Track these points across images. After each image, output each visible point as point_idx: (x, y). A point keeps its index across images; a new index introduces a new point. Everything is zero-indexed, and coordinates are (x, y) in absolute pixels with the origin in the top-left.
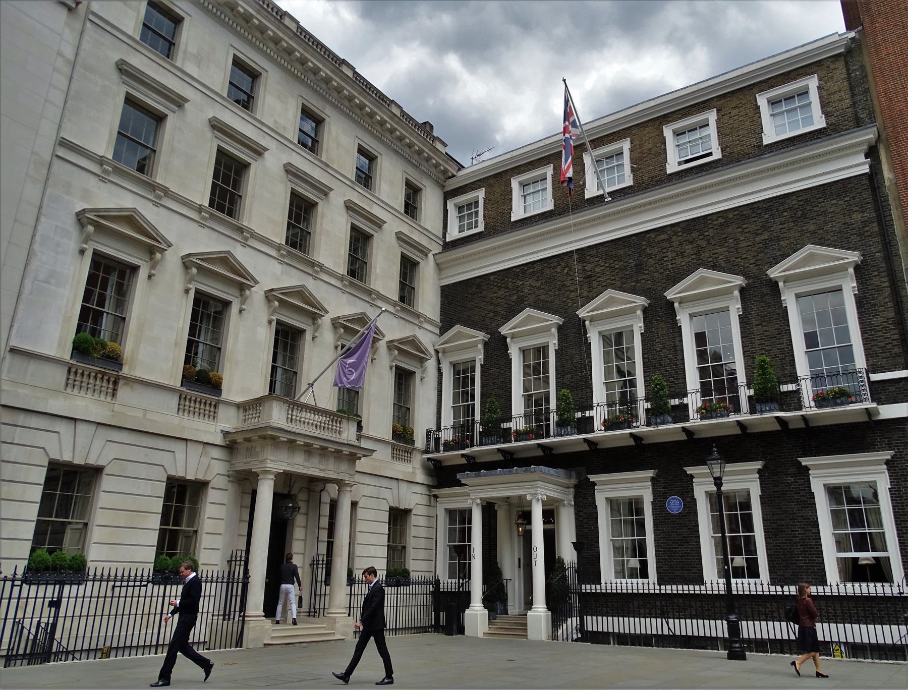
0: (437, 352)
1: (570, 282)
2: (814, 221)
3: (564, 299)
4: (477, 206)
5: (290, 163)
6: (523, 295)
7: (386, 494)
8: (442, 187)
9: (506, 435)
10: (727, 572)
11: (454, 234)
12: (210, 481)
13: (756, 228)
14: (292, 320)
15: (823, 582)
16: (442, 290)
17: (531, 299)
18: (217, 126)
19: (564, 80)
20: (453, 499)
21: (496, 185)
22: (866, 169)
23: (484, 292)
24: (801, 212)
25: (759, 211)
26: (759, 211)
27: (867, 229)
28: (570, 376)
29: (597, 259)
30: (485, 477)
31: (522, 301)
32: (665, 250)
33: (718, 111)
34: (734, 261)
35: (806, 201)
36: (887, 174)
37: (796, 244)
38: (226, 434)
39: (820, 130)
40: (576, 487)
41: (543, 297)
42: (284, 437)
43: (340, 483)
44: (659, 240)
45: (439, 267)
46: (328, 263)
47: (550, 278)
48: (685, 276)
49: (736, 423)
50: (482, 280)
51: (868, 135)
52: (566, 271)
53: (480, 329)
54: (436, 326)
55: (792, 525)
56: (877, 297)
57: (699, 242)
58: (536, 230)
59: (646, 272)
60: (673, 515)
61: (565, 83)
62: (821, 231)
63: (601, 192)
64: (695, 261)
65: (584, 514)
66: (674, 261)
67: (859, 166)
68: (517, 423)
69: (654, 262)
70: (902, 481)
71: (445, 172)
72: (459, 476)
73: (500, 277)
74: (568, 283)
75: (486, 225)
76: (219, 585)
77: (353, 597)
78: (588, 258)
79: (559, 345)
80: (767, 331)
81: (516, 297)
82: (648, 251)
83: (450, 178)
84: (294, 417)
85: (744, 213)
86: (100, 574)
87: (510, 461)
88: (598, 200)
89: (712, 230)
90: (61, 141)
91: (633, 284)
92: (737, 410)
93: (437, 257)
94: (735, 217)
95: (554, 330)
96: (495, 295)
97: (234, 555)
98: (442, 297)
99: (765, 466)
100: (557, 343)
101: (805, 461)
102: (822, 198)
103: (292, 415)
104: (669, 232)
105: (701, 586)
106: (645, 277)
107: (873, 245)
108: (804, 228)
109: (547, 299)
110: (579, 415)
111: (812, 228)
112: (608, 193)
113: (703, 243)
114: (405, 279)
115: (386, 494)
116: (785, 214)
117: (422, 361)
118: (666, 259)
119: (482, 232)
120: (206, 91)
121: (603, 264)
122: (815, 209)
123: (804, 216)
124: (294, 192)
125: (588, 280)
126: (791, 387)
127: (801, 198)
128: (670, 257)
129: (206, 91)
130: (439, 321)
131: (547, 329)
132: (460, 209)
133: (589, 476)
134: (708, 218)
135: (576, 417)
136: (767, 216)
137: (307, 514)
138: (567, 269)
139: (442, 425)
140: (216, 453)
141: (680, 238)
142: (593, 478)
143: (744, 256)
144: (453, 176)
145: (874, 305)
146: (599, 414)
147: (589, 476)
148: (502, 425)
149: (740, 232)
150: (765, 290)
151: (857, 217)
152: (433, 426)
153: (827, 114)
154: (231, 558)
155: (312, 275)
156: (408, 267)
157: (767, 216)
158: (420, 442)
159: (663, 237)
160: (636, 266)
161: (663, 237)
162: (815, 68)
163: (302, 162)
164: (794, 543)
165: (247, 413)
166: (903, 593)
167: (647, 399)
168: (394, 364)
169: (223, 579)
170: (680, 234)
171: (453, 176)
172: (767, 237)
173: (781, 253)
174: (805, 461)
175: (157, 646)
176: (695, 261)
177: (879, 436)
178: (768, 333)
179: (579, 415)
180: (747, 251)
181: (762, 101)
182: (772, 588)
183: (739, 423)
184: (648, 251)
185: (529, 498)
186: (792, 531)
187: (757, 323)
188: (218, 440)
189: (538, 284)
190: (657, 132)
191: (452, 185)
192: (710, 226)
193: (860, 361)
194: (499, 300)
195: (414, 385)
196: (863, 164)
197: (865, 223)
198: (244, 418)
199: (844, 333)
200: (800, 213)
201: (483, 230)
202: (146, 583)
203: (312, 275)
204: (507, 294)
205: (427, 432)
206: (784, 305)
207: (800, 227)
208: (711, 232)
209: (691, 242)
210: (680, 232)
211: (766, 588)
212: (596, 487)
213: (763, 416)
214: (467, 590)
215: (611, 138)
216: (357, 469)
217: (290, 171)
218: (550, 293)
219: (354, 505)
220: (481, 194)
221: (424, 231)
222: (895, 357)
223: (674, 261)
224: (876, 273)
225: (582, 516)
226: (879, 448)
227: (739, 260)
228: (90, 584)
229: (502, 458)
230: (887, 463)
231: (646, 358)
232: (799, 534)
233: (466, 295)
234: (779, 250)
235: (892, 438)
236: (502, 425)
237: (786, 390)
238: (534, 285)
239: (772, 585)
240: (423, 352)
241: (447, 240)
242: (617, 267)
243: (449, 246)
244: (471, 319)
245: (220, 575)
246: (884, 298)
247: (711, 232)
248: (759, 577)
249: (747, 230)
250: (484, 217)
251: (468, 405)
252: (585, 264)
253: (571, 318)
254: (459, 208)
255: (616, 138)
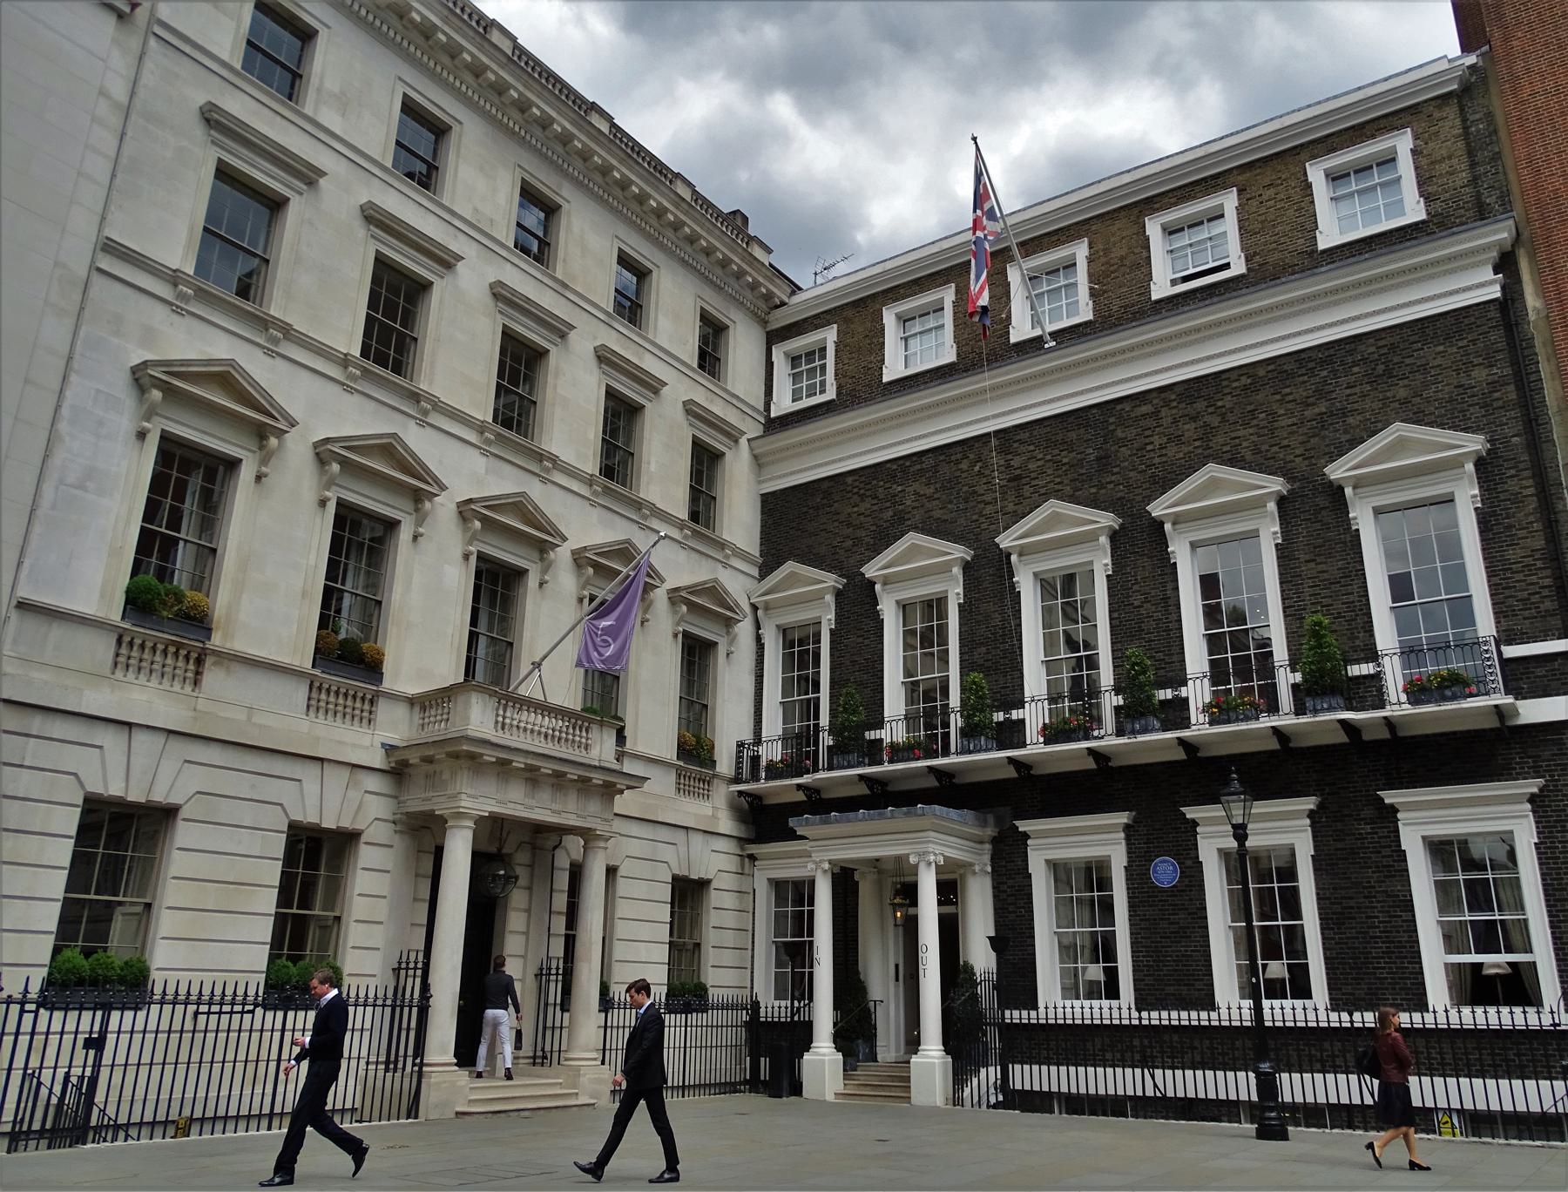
0: (755, 608)
1: (985, 487)
2: (1406, 382)
3: (975, 517)
4: (823, 357)
5: (500, 282)
6: (903, 510)
7: (667, 853)
8: (764, 322)
9: (874, 752)
10: (1256, 988)
11: (783, 403)
12: (363, 831)
13: (1305, 394)
14: (504, 554)
15: (1422, 1006)
16: (763, 502)
17: (918, 516)
18: (374, 218)
19: (974, 139)
20: (782, 861)
21: (857, 320)
22: (1495, 292)
23: (836, 505)
24: (1383, 367)
25: (1311, 365)
26: (1311, 365)
27: (1496, 395)
28: (984, 649)
29: (1032, 448)
30: (838, 825)
31: (902, 520)
32: (1148, 433)
33: (1240, 192)
34: (1267, 451)
35: (1393, 347)
36: (1532, 301)
37: (1375, 422)
38: (389, 749)
39: (1416, 224)
40: (995, 841)
41: (937, 514)
42: (490, 756)
43: (587, 834)
44: (1139, 414)
45: (758, 461)
46: (566, 455)
47: (950, 481)
48: (1183, 476)
49: (1271, 731)
50: (832, 483)
51: (1500, 233)
52: (977, 468)
53: (829, 569)
54: (753, 563)
55: (1367, 907)
56: (1514, 513)
57: (1208, 419)
58: (926, 398)
59: (1115, 470)
60: (1163, 890)
61: (976, 143)
62: (1418, 400)
63: (1038, 332)
64: (1200, 451)
65: (1009, 887)
66: (1164, 452)
67: (1483, 286)
68: (893, 731)
69: (1129, 452)
70: (1558, 832)
71: (768, 296)
72: (792, 822)
73: (863, 479)
74: (980, 489)
75: (839, 388)
76: (379, 1010)
77: (609, 1031)
78: (1015, 445)
79: (965, 596)
80: (1324, 572)
81: (891, 513)
82: (1119, 433)
83: (777, 307)
84: (508, 721)
85: (1285, 367)
86: (173, 991)
87: (880, 796)
88: (1033, 346)
89: (1229, 398)
90: (105, 244)
91: (1093, 490)
92: (1273, 708)
93: (754, 444)
94: (1270, 376)
95: (957, 571)
96: (856, 509)
97: (404, 959)
98: (763, 513)
99: (1321, 806)
100: (962, 593)
101: (1390, 797)
102: (1419, 342)
103: (504, 718)
104: (1155, 402)
105: (1211, 1013)
106: (1113, 478)
107: (1507, 424)
108: (1388, 394)
109: (945, 517)
110: (999, 717)
111: (1402, 393)
112: (1050, 334)
113: (1215, 421)
114: (699, 482)
115: (667, 853)
116: (1355, 369)
117: (729, 623)
118: (1149, 447)
119: (833, 400)
120: (356, 157)
121: (1041, 456)
122: (1408, 361)
123: (1388, 373)
124: (508, 331)
125: (1015, 483)
126: (1366, 669)
127: (1382, 343)
128: (1157, 443)
129: (356, 157)
130: (758, 555)
131: (944, 569)
132: (795, 360)
133: (1017, 823)
134: (1223, 377)
135: (995, 720)
136: (1325, 373)
137: (530, 888)
138: (979, 464)
139: (764, 735)
140: (373, 783)
141: (1174, 411)
142: (1024, 826)
143: (1285, 442)
144: (783, 304)
145: (1510, 527)
146: (1034, 716)
147: (1017, 823)
148: (867, 733)
149: (1278, 401)
150: (1322, 501)
151: (1480, 374)
152: (747, 736)
153: (1427, 197)
154: (400, 963)
155: (539, 476)
156: (705, 462)
157: (1325, 373)
158: (725, 763)
159: (1145, 409)
160: (1098, 459)
161: (1145, 409)
162: (1407, 118)
163: (522, 279)
164: (1371, 937)
165: (427, 714)
166: (1559, 1025)
167: (1117, 690)
168: (681, 629)
169: (384, 1001)
170: (1175, 404)
171: (783, 304)
172: (1324, 410)
173: (1348, 437)
174: (1390, 797)
175: (271, 1115)
176: (1200, 451)
177: (1518, 753)
178: (1326, 576)
179: (999, 717)
180: (1290, 433)
181: (1316, 174)
182: (1334, 1016)
183: (1276, 731)
184: (1119, 433)
185: (913, 860)
186: (1367, 917)
187: (1307, 557)
188: (377, 760)
189: (929, 491)
190: (1135, 229)
191: (780, 319)
192: (1226, 391)
193: (1485, 624)
194: (862, 518)
195: (715, 665)
196: (1491, 283)
197: (1494, 385)
198: (421, 722)
199: (1458, 575)
200: (1381, 368)
201: (834, 397)
202: (251, 1007)
203: (539, 476)
204: (875, 508)
205: (738, 746)
206: (1354, 528)
207: (1381, 392)
208: (1228, 402)
209: (1194, 419)
210: (1174, 400)
211: (1322, 1016)
212: (1029, 842)
213: (1317, 719)
214: (807, 1019)
215: (1055, 238)
216: (616, 811)
217: (501, 295)
218: (949, 506)
219: (611, 872)
220: (830, 335)
221: (733, 400)
222: (1545, 616)
223: (1164, 452)
224: (1513, 472)
225: (1005, 891)
226: (1517, 774)
227: (1276, 449)
228: (155, 1008)
229: (867, 792)
230: (1532, 799)
231: (1116, 618)
232: (1379, 922)
233: (805, 509)
234: (1346, 432)
235: (1540, 756)
236: (867, 733)
237: (1357, 673)
238: (922, 492)
239: (1333, 1010)
240: (730, 609)
241: (773, 415)
242: (1065, 460)
243: (775, 425)
244: (814, 551)
245: (380, 994)
246: (1527, 515)
247: (1228, 402)
248: (1310, 997)
249: (1291, 398)
250: (836, 375)
251: (809, 700)
252: (1010, 457)
253: (986, 550)
254: (793, 359)
255: (1064, 238)
